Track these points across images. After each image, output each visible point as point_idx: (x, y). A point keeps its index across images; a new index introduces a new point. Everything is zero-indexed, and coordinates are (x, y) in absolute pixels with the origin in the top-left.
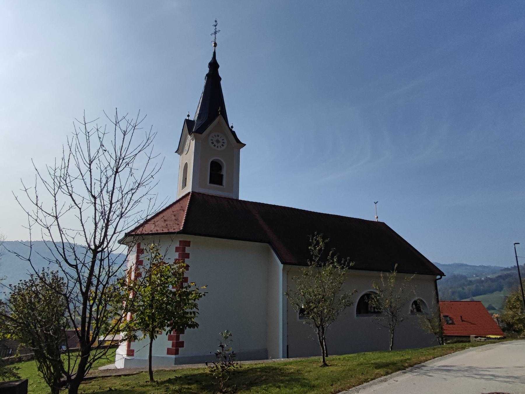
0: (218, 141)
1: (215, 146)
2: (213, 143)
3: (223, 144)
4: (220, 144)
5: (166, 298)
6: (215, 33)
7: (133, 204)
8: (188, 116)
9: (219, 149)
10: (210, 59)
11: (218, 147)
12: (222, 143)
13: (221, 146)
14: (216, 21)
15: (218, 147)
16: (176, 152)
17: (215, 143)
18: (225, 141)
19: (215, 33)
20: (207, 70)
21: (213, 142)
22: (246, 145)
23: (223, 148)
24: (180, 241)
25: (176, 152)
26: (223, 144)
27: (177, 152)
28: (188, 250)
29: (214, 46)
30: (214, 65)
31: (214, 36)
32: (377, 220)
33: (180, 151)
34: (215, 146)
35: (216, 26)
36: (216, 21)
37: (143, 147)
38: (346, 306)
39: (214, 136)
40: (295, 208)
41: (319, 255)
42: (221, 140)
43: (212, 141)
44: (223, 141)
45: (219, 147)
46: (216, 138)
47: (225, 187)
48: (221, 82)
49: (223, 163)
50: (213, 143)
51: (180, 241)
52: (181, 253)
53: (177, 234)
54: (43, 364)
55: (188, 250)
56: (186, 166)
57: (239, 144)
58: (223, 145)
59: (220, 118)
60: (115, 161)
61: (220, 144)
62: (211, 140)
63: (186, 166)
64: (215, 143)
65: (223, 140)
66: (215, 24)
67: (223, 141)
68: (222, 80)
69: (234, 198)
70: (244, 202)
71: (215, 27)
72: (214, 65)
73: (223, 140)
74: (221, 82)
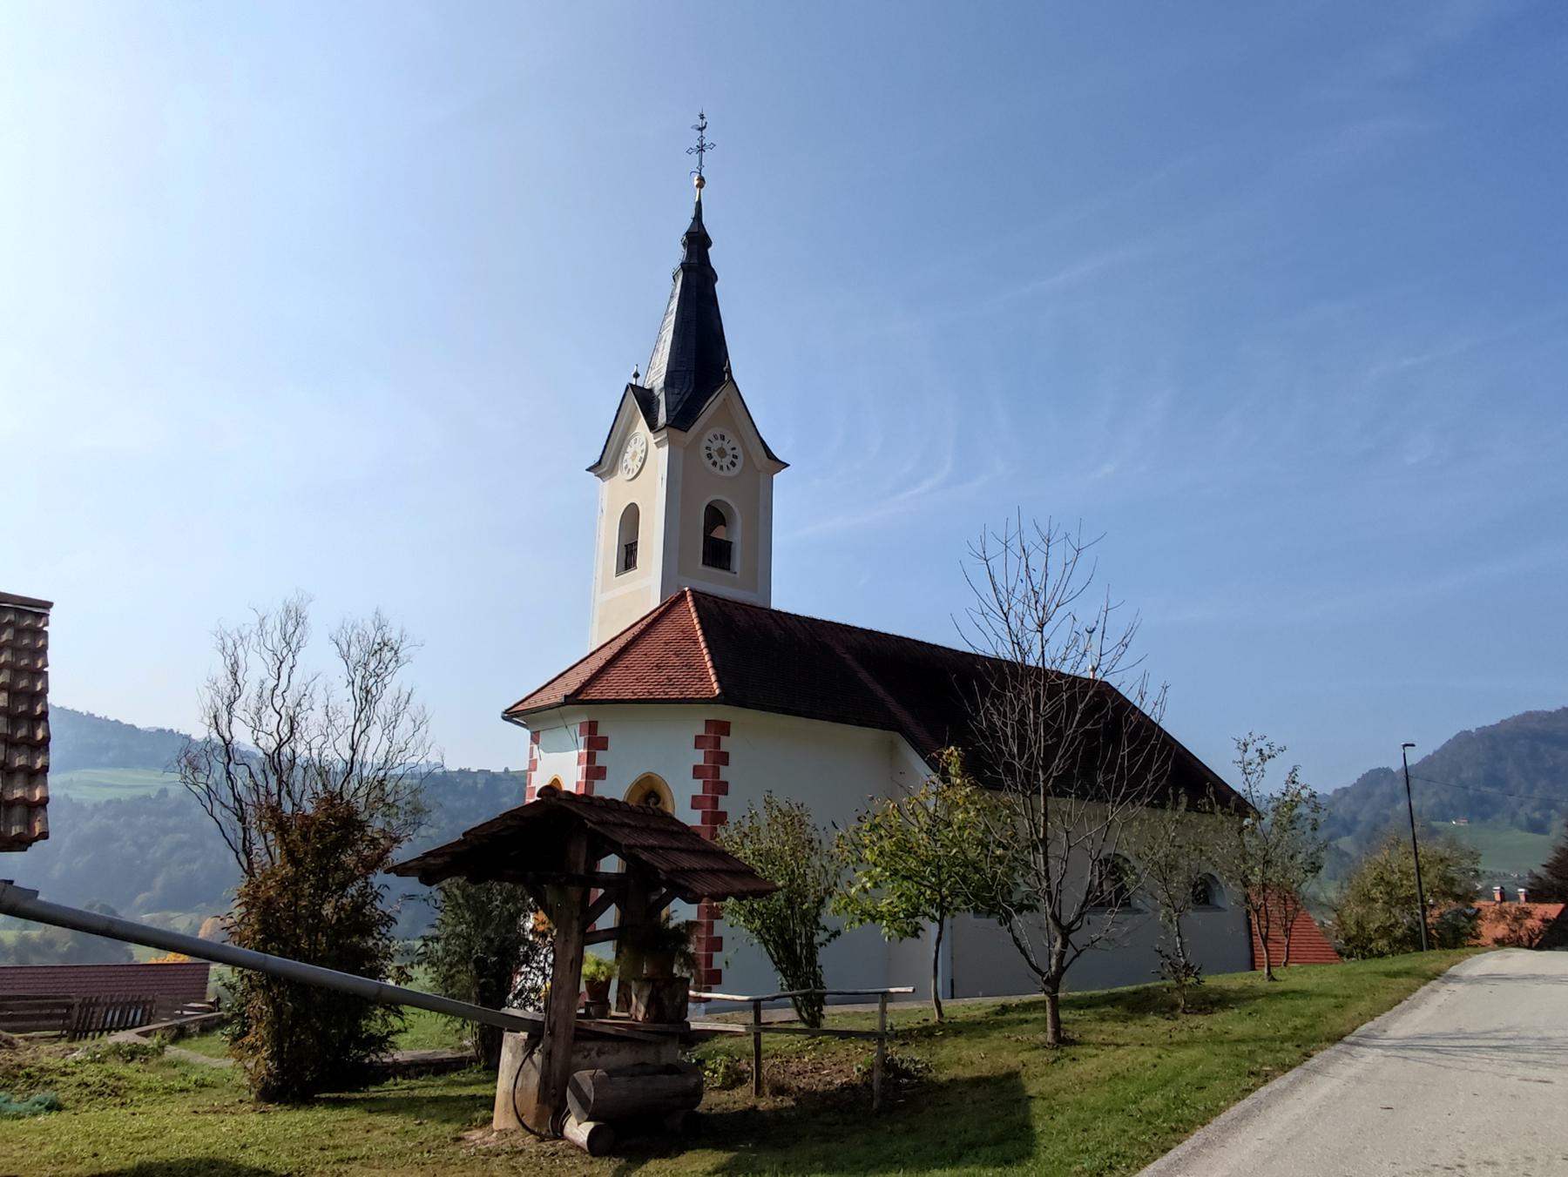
0: (722, 453)
1: (715, 464)
2: (710, 456)
4: (726, 461)
5: (582, 873)
6: (701, 149)
8: (636, 375)
9: (725, 473)
10: (686, 223)
11: (721, 468)
13: (730, 466)
14: (702, 117)
15: (721, 468)
17: (716, 457)
18: (739, 452)
19: (701, 149)
20: (678, 254)
21: (710, 454)
22: (788, 465)
23: (735, 471)
24: (707, 721)
27: (597, 469)
28: (726, 744)
29: (697, 186)
30: (697, 241)
31: (696, 156)
32: (1094, 676)
33: (604, 470)
34: (715, 464)
35: (701, 129)
36: (702, 117)
38: (87, 1085)
39: (713, 439)
40: (848, 623)
42: (729, 451)
43: (709, 452)
44: (735, 452)
46: (717, 444)
47: (738, 575)
48: (717, 286)
49: (733, 511)
50: (710, 456)
51: (707, 721)
52: (710, 752)
55: (726, 744)
56: (631, 517)
57: (771, 461)
58: (733, 464)
61: (726, 461)
62: (707, 448)
63: (631, 517)
64: (716, 457)
65: (733, 449)
66: (700, 123)
68: (1532, 709)
69: (760, 604)
70: (779, 612)
71: (700, 132)
72: (697, 241)
73: (733, 449)
74: (716, 286)
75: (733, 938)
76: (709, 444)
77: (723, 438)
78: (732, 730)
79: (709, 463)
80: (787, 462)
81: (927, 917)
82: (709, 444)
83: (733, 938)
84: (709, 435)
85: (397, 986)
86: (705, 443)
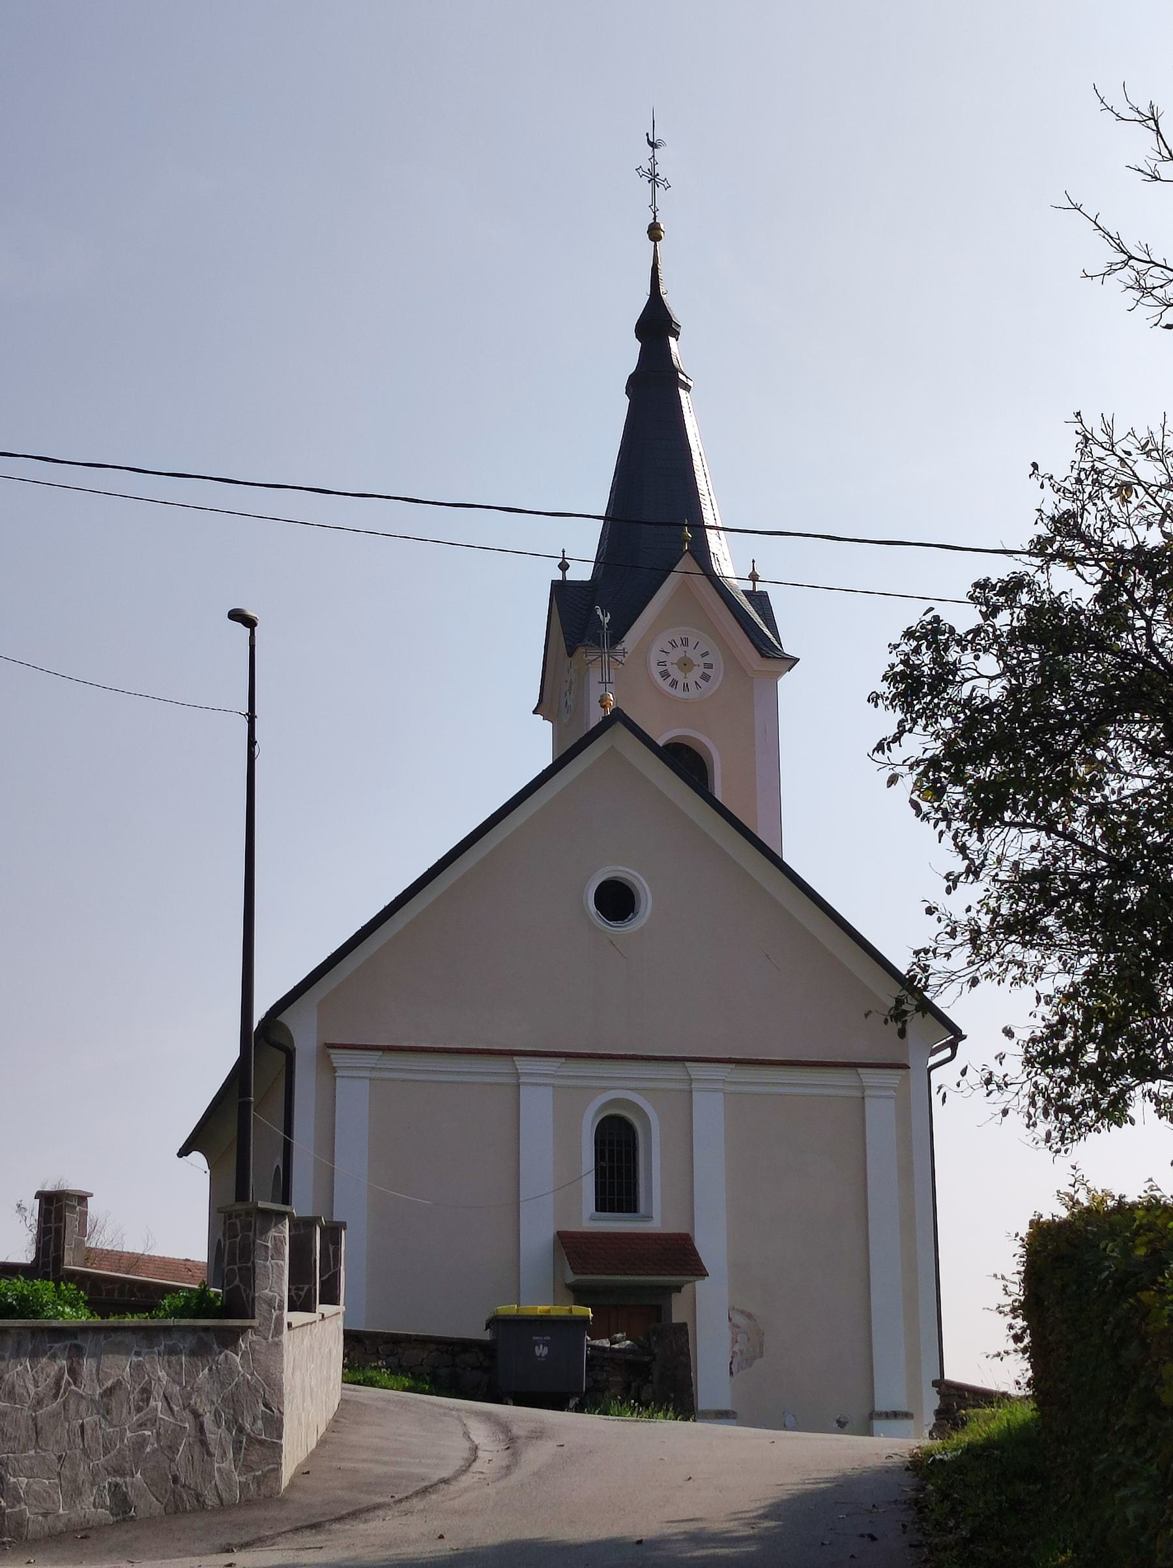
1: (674, 684)
2: (665, 675)
3: (708, 671)
4: (695, 675)
7: (1051, 578)
11: (686, 687)
12: (701, 670)
13: (701, 682)
15: (686, 687)
16: (535, 712)
17: (676, 673)
18: (716, 658)
25: (535, 712)
26: (708, 671)
37: (1166, 147)
39: (668, 648)
41: (104, 1294)
43: (663, 668)
44: (707, 660)
45: (692, 686)
46: (677, 654)
50: (665, 675)
53: (285, 1140)
54: (1095, 1229)
59: (686, 563)
60: (1154, 134)
61: (695, 675)
64: (676, 673)
67: (707, 660)
75: (441, 1537)
76: (663, 657)
77: (685, 642)
78: (73, 1184)
79: (664, 685)
80: (876, 1536)
81: (889, 669)
82: (663, 657)
83: (441, 1537)
84: (662, 642)
85: (617, 1224)
86: (655, 656)
